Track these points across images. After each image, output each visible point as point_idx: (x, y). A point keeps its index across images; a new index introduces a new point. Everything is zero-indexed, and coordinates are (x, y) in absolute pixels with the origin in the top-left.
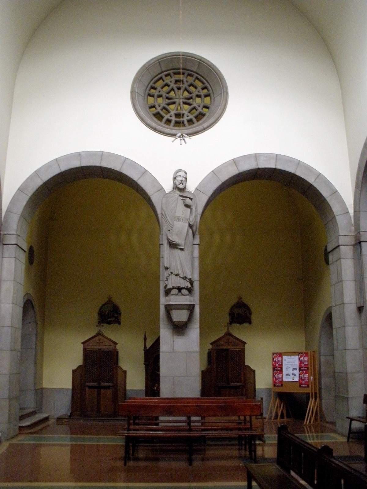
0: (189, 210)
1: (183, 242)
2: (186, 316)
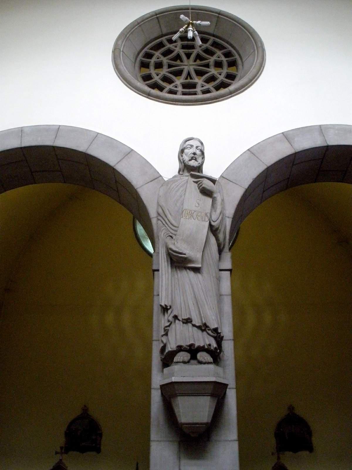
0: (209, 200)
1: (199, 256)
2: (207, 409)
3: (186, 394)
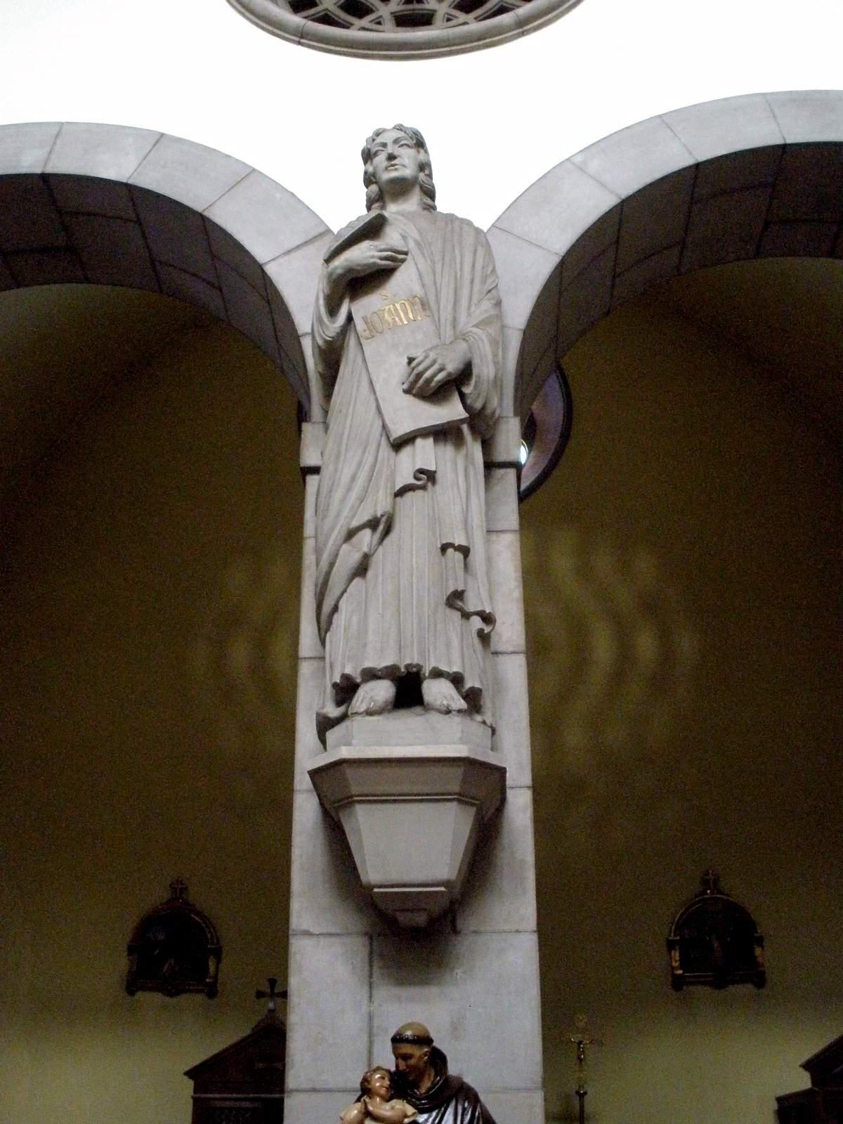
3: (340, 801)
